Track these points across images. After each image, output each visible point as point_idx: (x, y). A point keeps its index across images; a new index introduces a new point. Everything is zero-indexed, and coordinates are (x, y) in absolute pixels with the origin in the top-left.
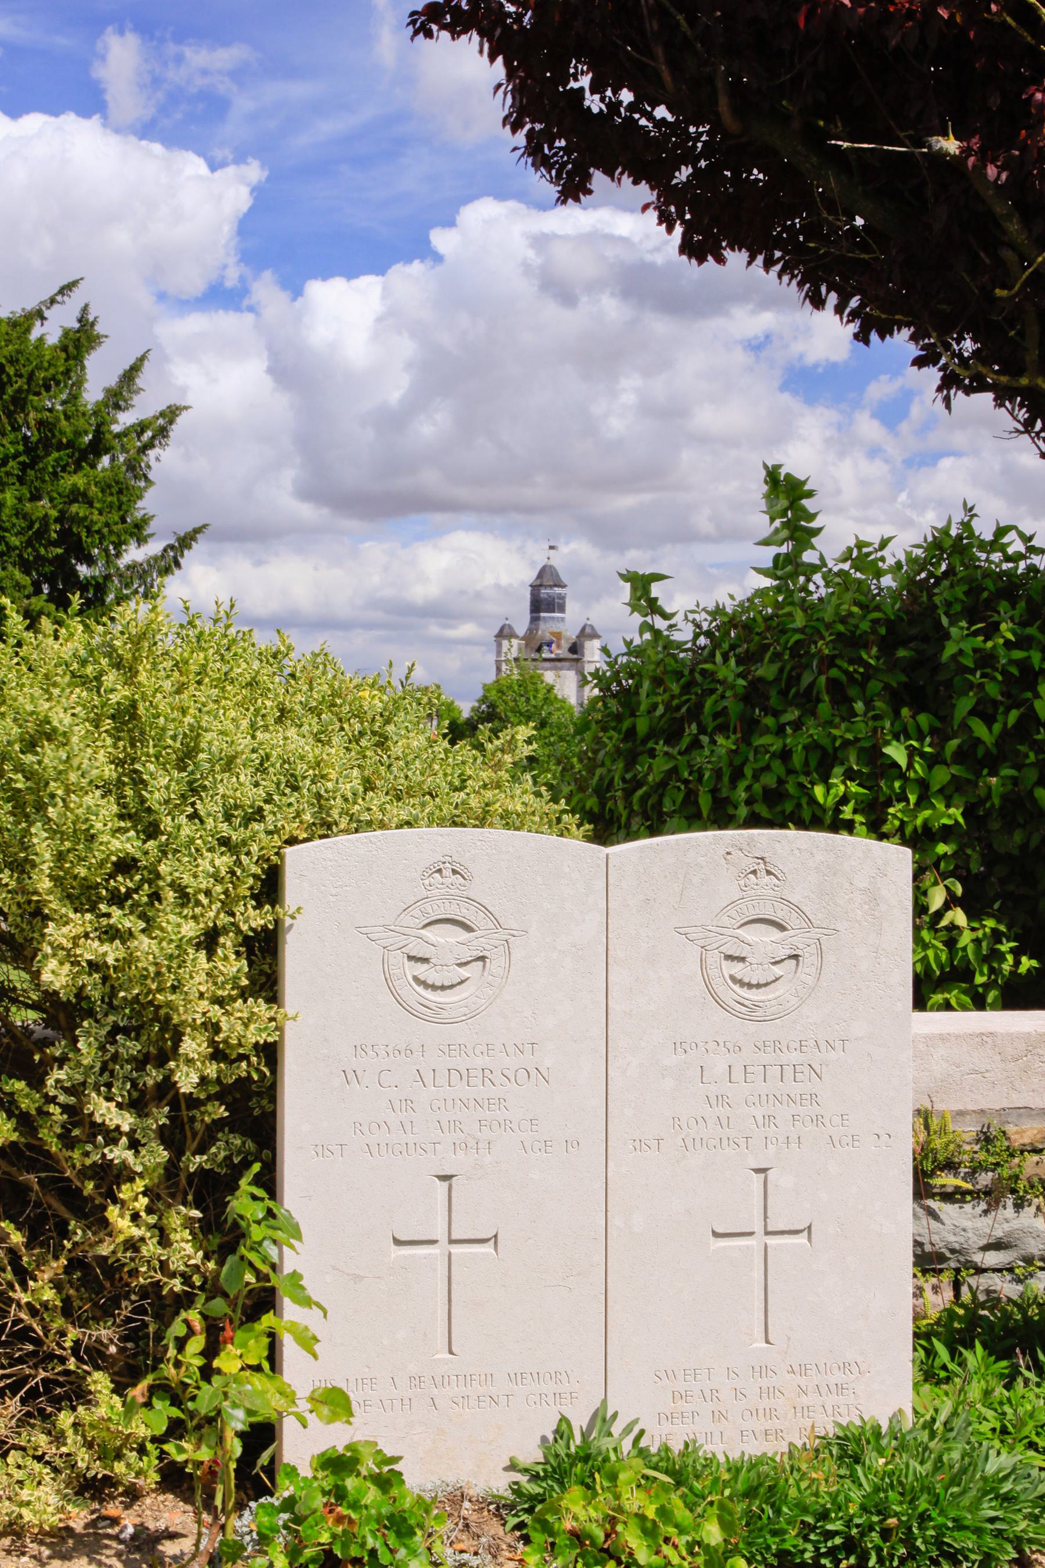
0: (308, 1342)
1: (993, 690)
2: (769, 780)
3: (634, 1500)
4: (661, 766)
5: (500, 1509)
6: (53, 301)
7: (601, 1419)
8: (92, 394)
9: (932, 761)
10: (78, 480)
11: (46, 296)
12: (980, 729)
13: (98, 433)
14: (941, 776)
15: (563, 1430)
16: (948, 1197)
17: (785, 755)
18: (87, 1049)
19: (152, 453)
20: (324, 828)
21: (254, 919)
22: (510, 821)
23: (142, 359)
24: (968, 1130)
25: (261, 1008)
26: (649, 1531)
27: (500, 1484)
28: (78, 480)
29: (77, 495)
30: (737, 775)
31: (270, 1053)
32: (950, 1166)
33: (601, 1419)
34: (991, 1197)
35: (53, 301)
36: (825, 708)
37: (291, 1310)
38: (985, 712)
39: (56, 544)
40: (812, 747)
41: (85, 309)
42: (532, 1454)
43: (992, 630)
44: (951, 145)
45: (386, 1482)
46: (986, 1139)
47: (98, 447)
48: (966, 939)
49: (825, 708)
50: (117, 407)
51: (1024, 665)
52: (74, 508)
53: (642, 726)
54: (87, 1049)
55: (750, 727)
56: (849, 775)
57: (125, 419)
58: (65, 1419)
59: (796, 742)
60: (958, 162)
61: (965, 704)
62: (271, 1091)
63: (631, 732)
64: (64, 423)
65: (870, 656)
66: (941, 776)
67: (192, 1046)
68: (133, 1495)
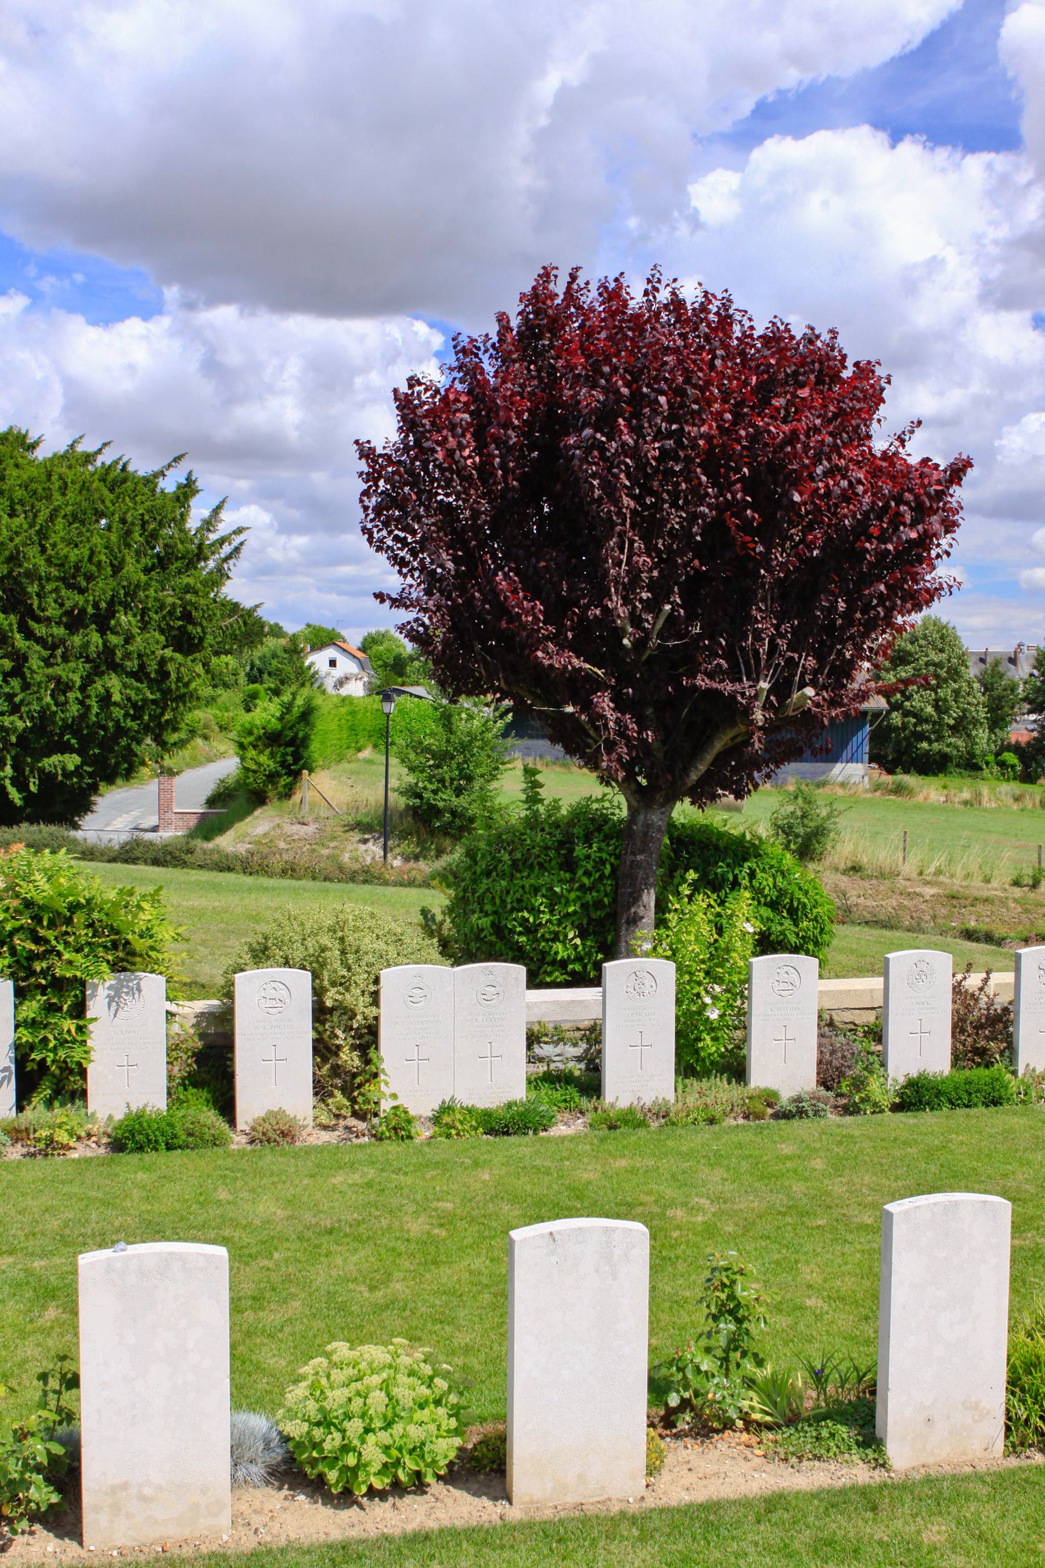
0: (387, 1083)
1: (589, 867)
2: (518, 895)
3: (458, 1116)
4: (483, 887)
5: (430, 1119)
6: (169, 466)
7: (452, 1099)
8: (193, 523)
9: (569, 891)
10: (186, 580)
11: (166, 463)
12: (585, 880)
13: (200, 547)
14: (573, 895)
15: (444, 1102)
16: (546, 1043)
17: (523, 887)
18: (335, 1019)
19: (231, 562)
20: (389, 966)
21: (372, 988)
22: (431, 962)
23: (223, 502)
24: (552, 1025)
25: (374, 1008)
26: (461, 1123)
27: (430, 1114)
28: (186, 580)
29: (188, 589)
30: (508, 893)
31: (376, 1018)
32: (546, 1035)
33: (452, 1099)
34: (556, 1043)
35: (169, 466)
36: (536, 870)
37: (382, 1077)
38: (587, 873)
39: (178, 619)
40: (531, 886)
41: (190, 473)
42: (437, 1108)
43: (591, 847)
44: (570, 709)
45: (406, 1112)
46: (556, 1028)
47: (200, 555)
48: (580, 948)
49: (536, 870)
50: (209, 530)
51: (600, 858)
52: (188, 596)
53: (478, 871)
54: (335, 1019)
55: (512, 877)
56: (543, 896)
57: (213, 537)
58: (330, 1101)
59: (527, 883)
60: (573, 714)
61: (580, 872)
62: (377, 1026)
63: (475, 873)
64: (180, 546)
65: (552, 853)
66: (573, 895)
67: (359, 1017)
68: (345, 1118)
